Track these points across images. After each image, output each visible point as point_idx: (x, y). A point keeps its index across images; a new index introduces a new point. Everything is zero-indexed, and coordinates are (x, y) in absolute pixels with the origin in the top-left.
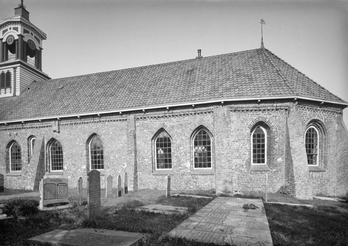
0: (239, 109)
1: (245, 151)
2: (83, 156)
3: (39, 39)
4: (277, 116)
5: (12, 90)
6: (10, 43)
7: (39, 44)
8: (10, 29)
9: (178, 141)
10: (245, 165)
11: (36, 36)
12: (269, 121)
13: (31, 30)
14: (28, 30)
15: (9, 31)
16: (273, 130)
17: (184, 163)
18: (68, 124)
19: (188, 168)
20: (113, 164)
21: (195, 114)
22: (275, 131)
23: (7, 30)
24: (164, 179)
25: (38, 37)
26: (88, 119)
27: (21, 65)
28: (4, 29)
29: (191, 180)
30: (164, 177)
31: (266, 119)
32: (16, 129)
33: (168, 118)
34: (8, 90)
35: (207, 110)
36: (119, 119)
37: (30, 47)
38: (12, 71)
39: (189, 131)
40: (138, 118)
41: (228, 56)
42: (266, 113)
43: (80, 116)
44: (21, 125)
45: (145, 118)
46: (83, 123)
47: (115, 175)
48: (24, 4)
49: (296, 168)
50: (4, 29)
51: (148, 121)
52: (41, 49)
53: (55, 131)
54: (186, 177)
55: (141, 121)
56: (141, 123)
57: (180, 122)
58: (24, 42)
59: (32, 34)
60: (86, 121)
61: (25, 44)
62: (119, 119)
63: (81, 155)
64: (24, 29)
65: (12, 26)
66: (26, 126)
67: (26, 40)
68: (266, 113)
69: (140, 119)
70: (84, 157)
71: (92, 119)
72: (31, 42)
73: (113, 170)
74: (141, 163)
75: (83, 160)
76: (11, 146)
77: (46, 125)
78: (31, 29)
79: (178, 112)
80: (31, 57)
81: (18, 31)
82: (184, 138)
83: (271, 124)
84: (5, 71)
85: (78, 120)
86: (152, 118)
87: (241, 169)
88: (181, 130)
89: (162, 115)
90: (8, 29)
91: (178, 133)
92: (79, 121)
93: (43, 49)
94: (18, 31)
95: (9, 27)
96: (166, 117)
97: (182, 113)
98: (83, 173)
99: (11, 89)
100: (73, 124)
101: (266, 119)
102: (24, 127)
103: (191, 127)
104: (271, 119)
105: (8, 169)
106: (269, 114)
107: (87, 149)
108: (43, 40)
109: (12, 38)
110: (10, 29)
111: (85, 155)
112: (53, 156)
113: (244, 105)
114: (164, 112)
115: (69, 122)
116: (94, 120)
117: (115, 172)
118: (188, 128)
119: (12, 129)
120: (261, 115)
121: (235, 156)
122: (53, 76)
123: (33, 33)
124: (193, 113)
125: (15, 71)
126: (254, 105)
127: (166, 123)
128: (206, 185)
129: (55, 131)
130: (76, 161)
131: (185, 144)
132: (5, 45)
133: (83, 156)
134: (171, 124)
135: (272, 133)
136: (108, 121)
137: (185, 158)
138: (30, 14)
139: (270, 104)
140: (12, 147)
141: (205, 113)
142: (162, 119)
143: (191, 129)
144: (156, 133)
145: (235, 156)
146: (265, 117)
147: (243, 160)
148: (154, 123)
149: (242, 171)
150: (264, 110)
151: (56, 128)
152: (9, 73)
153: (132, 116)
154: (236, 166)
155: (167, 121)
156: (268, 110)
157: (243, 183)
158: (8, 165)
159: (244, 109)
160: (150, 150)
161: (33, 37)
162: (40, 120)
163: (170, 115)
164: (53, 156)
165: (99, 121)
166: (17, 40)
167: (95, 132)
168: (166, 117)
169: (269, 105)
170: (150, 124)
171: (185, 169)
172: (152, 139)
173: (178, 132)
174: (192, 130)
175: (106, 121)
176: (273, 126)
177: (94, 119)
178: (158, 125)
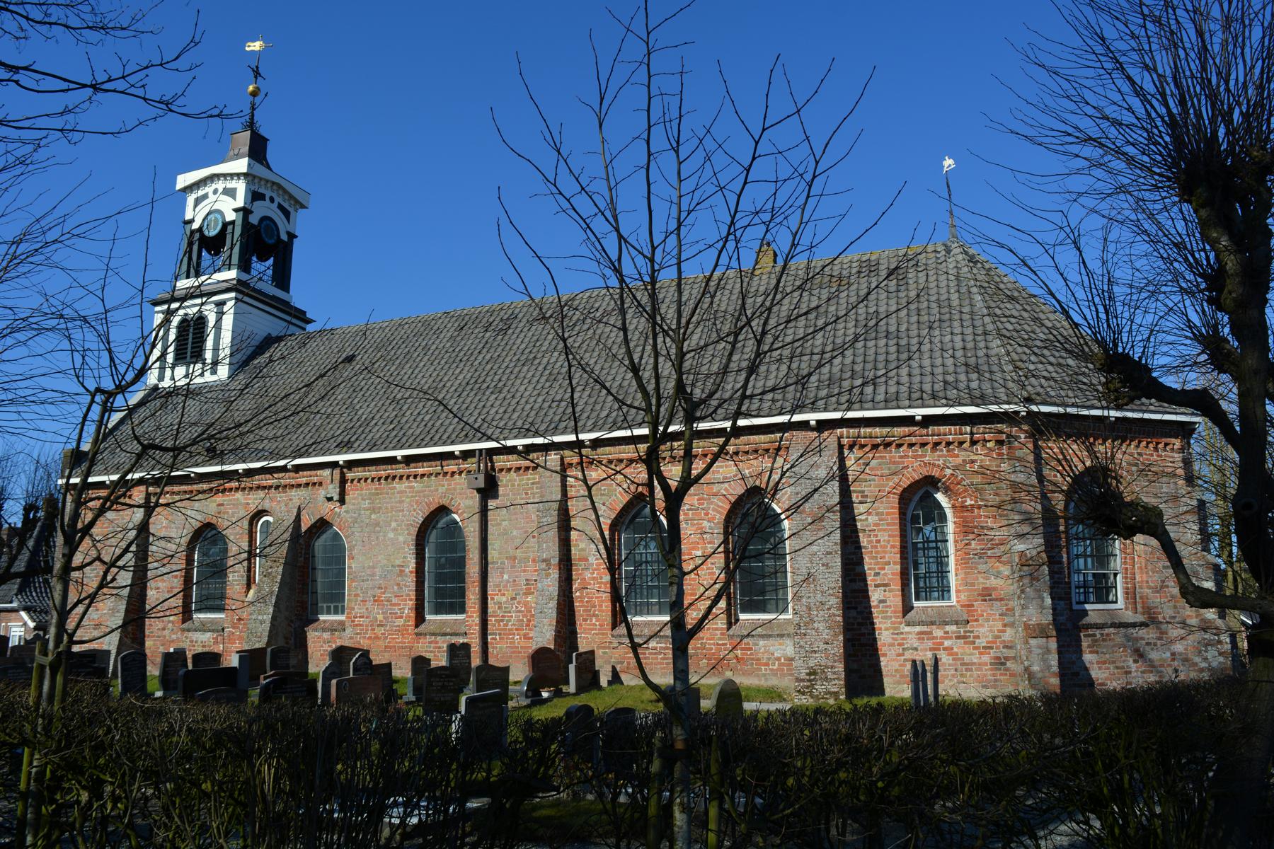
6: (212, 232)
11: (283, 203)
15: (212, 198)
23: (205, 196)
25: (286, 205)
26: (425, 464)
27: (240, 296)
28: (201, 193)
42: (942, 450)
43: (345, 461)
48: (256, 119)
50: (201, 193)
52: (292, 236)
53: (330, 499)
54: (714, 644)
59: (272, 200)
60: (420, 471)
63: (402, 571)
64: (288, 292)
65: (220, 185)
66: (246, 482)
68: (942, 450)
71: (439, 463)
75: (406, 586)
77: (304, 480)
79: (646, 655)
81: (235, 199)
85: (397, 466)
90: (211, 194)
92: (401, 470)
93: (296, 237)
94: (235, 199)
95: (214, 186)
109: (219, 217)
110: (215, 192)
111: (411, 572)
113: (877, 431)
114: (857, 430)
115: (371, 472)
122: (320, 316)
125: (220, 314)
126: (906, 430)
129: (330, 499)
130: (386, 588)
139: (953, 428)
146: (941, 462)
150: (937, 444)
152: (201, 321)
156: (948, 444)
162: (457, 453)
165: (459, 469)
166: (233, 223)
167: (445, 502)
169: (950, 430)
177: (444, 463)
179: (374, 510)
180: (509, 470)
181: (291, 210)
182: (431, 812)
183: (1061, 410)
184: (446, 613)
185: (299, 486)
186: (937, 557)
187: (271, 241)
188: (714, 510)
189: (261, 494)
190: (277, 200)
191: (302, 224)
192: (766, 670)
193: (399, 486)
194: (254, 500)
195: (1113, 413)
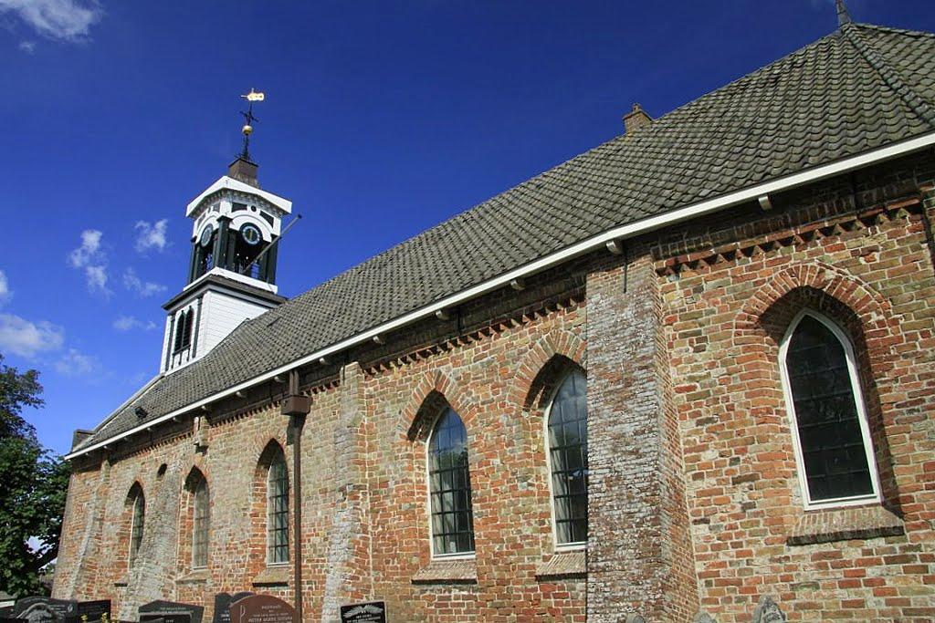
4: (874, 249)
12: (838, 279)
16: (869, 317)
22: (880, 323)
24: (449, 598)
31: (822, 271)
41: (830, 128)
59: (254, 209)
67: (236, 226)
78: (239, 196)
82: (503, 419)
83: (851, 290)
84: (186, 309)
88: (493, 388)
91: (483, 403)
101: (822, 271)
104: (846, 271)
106: (831, 250)
118: (511, 377)
120: (792, 261)
127: (443, 369)
131: (508, 446)
132: (198, 249)
135: (871, 335)
143: (521, 378)
148: (411, 379)
167: (273, 435)
171: (512, 554)
172: (530, 398)
174: (524, 379)
176: (867, 299)
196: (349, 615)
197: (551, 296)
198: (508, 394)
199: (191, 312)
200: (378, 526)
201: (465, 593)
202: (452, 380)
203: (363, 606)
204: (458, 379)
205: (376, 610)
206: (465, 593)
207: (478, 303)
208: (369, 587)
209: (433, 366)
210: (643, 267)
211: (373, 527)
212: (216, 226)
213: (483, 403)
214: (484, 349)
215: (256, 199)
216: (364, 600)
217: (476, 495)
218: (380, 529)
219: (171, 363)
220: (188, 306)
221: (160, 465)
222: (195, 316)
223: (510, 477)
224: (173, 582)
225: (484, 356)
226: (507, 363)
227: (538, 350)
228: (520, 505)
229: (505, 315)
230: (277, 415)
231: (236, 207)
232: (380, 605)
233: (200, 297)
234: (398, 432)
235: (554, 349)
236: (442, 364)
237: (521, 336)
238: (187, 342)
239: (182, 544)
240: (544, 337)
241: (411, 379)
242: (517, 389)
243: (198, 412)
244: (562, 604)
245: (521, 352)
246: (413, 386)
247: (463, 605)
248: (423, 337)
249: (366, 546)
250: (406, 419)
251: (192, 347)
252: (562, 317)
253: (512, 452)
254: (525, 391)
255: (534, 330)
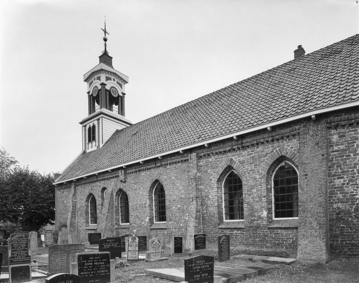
0: (343, 123)
1: (355, 190)
2: (146, 207)
3: (121, 83)
5: (97, 143)
7: (122, 89)
8: (95, 79)
9: (250, 182)
10: (354, 212)
11: (119, 81)
13: (113, 76)
14: (110, 76)
15: (94, 82)
17: (259, 212)
18: (133, 172)
19: (264, 218)
20: (175, 215)
21: (273, 141)
23: (92, 82)
24: (233, 234)
25: (120, 82)
29: (267, 236)
30: (233, 232)
32: (92, 182)
33: (237, 151)
34: (94, 143)
35: (290, 132)
36: (180, 159)
37: (113, 94)
38: (96, 123)
39: (263, 168)
40: (201, 156)
44: (96, 177)
45: (209, 155)
46: (146, 169)
47: (178, 228)
48: (107, 50)
49: (231, 250)
51: (212, 159)
54: (262, 232)
55: (205, 159)
56: (205, 162)
57: (252, 154)
58: (106, 90)
59: (114, 80)
61: (108, 93)
62: (180, 160)
63: (145, 206)
67: (108, 87)
69: (203, 157)
70: (147, 208)
72: (113, 89)
73: (175, 222)
74: (205, 213)
76: (90, 199)
77: (114, 176)
78: (108, 73)
79: (249, 141)
80: (116, 105)
82: (258, 177)
84: (91, 125)
86: (216, 153)
87: (348, 220)
88: (254, 166)
89: (228, 149)
96: (234, 150)
97: (255, 142)
98: (147, 226)
99: (96, 142)
100: (137, 171)
102: (99, 179)
103: (267, 159)
105: (87, 222)
107: (151, 199)
108: (126, 84)
112: (161, 206)
116: (156, 164)
117: (177, 225)
118: (262, 162)
119: (90, 183)
121: (336, 199)
123: (115, 78)
124: (270, 139)
125: (98, 123)
127: (233, 158)
128: (290, 242)
131: (259, 185)
132: (91, 97)
133: (146, 207)
134: (242, 159)
136: (170, 164)
137: (260, 205)
138: (113, 59)
140: (91, 200)
141: (288, 137)
142: (229, 154)
143: (267, 163)
144: (222, 174)
145: (336, 199)
147: (351, 205)
148: (219, 161)
149: (349, 222)
151: (122, 177)
153: (194, 155)
154: (337, 214)
155: (235, 155)
157: (351, 241)
158: (87, 218)
159: (353, 121)
160: (215, 196)
161: (115, 82)
163: (239, 146)
164: (161, 206)
166: (100, 90)
167: (157, 178)
168: (234, 150)
170: (215, 161)
173: (249, 170)
175: (167, 164)
178: (224, 162)
179: (136, 183)
180: (179, 162)
181: (122, 84)
182: (195, 271)
183: (353, 141)
184: (14, 267)
185: (114, 177)
186: (27, 240)
187: (116, 96)
188: (262, 170)
189: (103, 182)
190: (116, 80)
191: (127, 89)
192: (286, 243)
193: (143, 174)
194: (102, 184)
195: (277, 187)
196: (196, 238)
197: (282, 134)
198: (261, 168)
199: (94, 126)
200: (204, 211)
201: (240, 232)
202: (237, 162)
203: (200, 235)
204: (239, 162)
205: (203, 237)
206: (240, 232)
207: (250, 135)
208: (201, 230)
209: (229, 156)
210: (322, 125)
211: (202, 211)
212: (100, 87)
213: (250, 171)
214: (252, 151)
215: (115, 75)
216: (200, 234)
217: (246, 201)
218: (205, 211)
219: (87, 147)
220: (93, 123)
221: (102, 188)
222: (97, 128)
223: (260, 196)
224: (115, 229)
225: (252, 154)
226: (261, 157)
227: (275, 153)
228: (263, 205)
229: (262, 140)
230: (173, 174)
231: (108, 79)
232: (204, 235)
233: (98, 120)
234: (213, 179)
235: (281, 153)
236: (233, 156)
237: (268, 148)
238: (94, 139)
239: (116, 216)
240: (278, 149)
241: (219, 161)
242: (264, 166)
243: (121, 168)
244: (277, 236)
245: (267, 154)
246: (220, 163)
247: (238, 236)
248: (225, 145)
249: (200, 216)
250: (217, 175)
251: (97, 141)
252: (286, 142)
253: (261, 187)
254: (268, 168)
255: (274, 146)
